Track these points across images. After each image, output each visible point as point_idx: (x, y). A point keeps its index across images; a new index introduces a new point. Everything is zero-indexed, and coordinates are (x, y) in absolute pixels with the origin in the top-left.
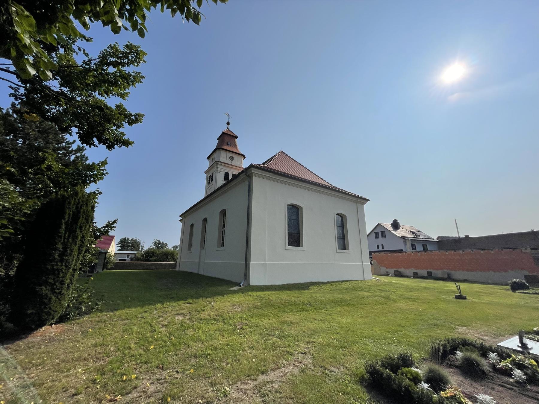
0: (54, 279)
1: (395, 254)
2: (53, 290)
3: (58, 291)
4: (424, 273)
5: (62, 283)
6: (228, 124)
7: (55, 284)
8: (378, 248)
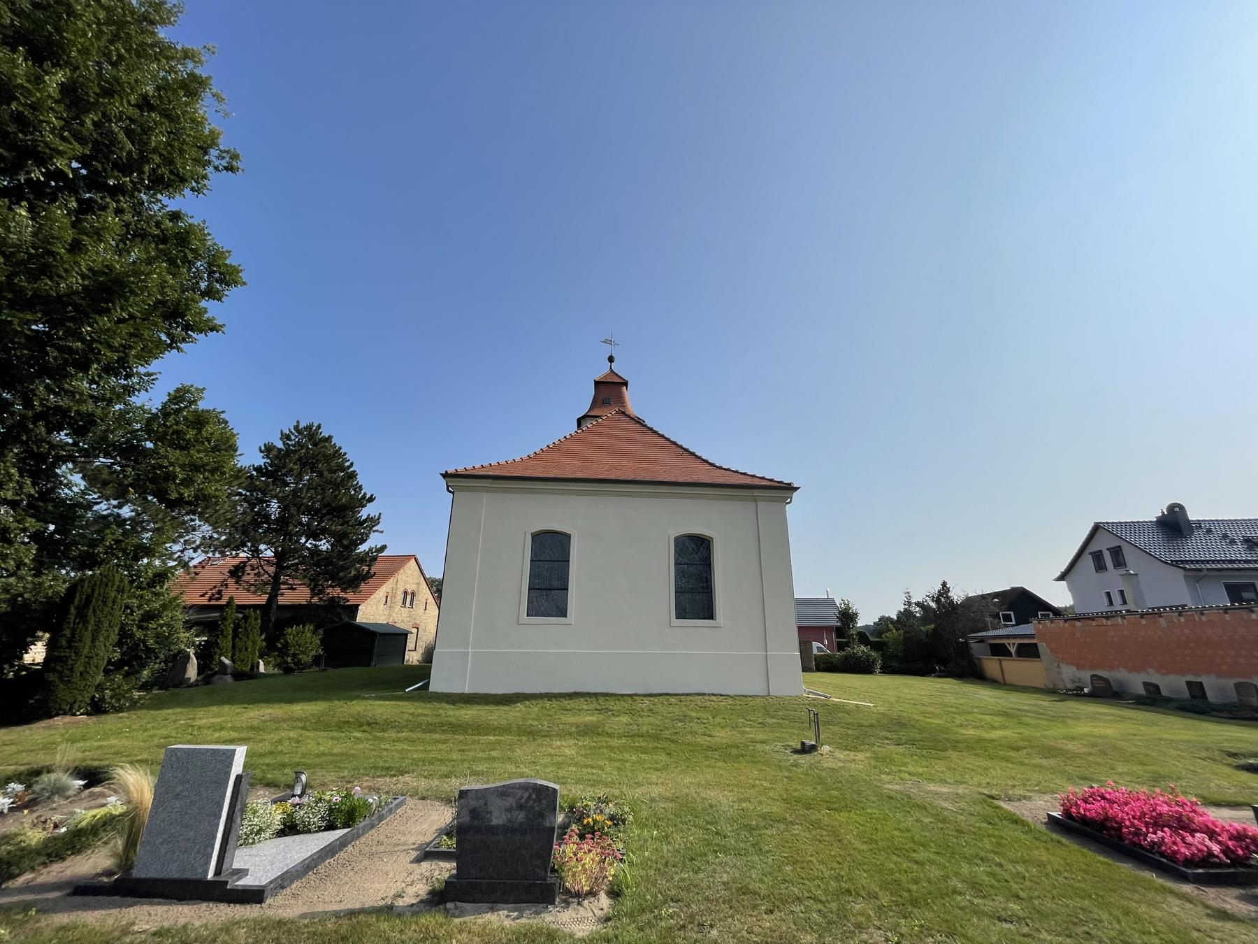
0: (62, 667)
1: (1094, 623)
2: (61, 677)
3: (66, 679)
4: (1173, 684)
5: (71, 670)
6: (611, 359)
7: (63, 672)
8: (1111, 603)
